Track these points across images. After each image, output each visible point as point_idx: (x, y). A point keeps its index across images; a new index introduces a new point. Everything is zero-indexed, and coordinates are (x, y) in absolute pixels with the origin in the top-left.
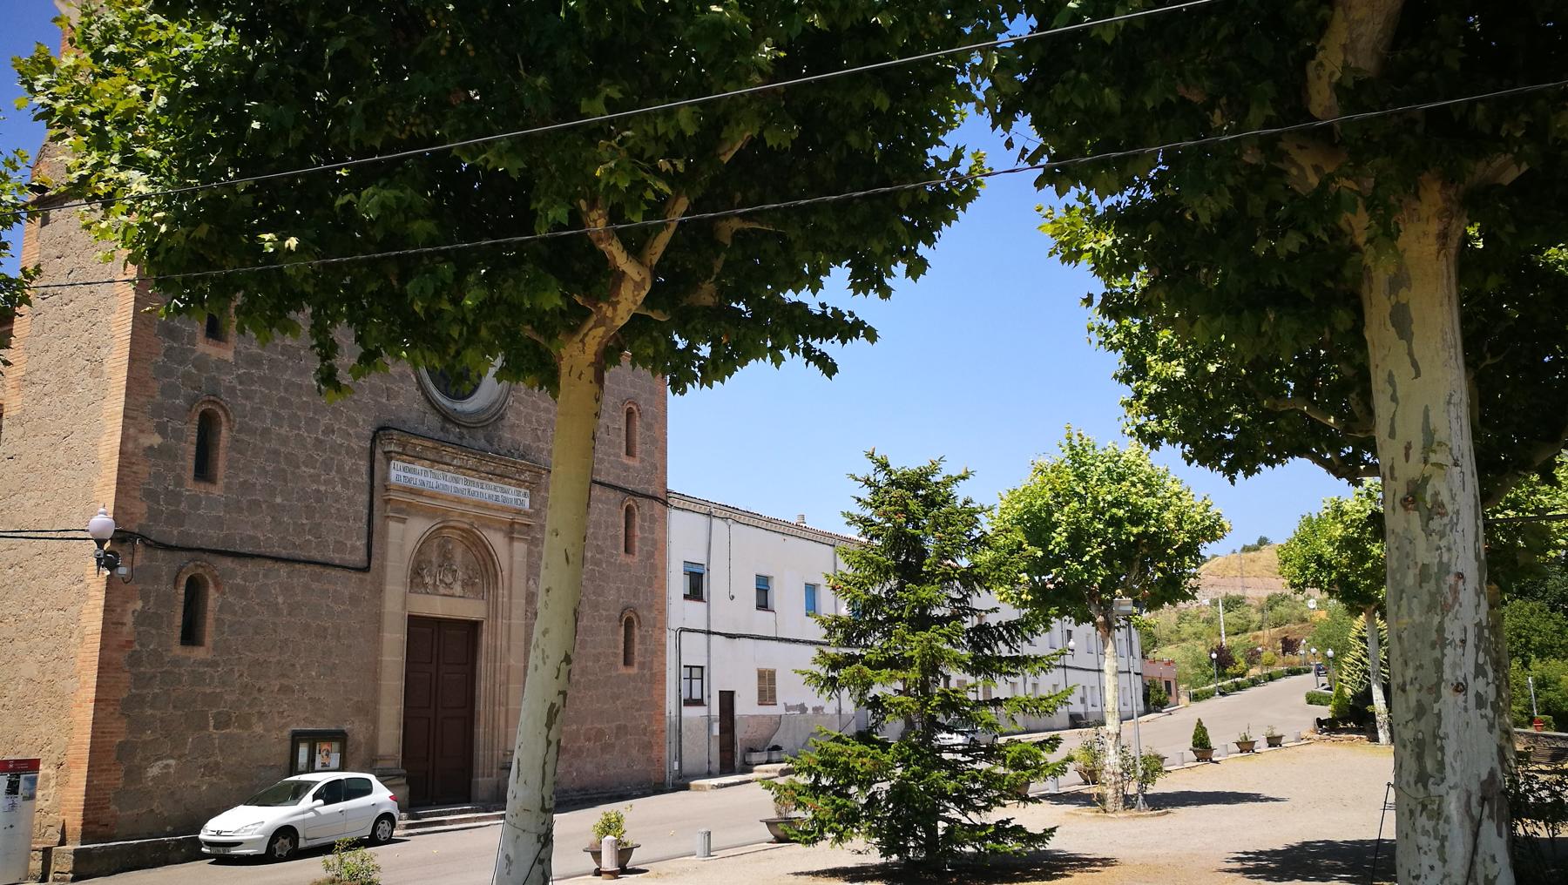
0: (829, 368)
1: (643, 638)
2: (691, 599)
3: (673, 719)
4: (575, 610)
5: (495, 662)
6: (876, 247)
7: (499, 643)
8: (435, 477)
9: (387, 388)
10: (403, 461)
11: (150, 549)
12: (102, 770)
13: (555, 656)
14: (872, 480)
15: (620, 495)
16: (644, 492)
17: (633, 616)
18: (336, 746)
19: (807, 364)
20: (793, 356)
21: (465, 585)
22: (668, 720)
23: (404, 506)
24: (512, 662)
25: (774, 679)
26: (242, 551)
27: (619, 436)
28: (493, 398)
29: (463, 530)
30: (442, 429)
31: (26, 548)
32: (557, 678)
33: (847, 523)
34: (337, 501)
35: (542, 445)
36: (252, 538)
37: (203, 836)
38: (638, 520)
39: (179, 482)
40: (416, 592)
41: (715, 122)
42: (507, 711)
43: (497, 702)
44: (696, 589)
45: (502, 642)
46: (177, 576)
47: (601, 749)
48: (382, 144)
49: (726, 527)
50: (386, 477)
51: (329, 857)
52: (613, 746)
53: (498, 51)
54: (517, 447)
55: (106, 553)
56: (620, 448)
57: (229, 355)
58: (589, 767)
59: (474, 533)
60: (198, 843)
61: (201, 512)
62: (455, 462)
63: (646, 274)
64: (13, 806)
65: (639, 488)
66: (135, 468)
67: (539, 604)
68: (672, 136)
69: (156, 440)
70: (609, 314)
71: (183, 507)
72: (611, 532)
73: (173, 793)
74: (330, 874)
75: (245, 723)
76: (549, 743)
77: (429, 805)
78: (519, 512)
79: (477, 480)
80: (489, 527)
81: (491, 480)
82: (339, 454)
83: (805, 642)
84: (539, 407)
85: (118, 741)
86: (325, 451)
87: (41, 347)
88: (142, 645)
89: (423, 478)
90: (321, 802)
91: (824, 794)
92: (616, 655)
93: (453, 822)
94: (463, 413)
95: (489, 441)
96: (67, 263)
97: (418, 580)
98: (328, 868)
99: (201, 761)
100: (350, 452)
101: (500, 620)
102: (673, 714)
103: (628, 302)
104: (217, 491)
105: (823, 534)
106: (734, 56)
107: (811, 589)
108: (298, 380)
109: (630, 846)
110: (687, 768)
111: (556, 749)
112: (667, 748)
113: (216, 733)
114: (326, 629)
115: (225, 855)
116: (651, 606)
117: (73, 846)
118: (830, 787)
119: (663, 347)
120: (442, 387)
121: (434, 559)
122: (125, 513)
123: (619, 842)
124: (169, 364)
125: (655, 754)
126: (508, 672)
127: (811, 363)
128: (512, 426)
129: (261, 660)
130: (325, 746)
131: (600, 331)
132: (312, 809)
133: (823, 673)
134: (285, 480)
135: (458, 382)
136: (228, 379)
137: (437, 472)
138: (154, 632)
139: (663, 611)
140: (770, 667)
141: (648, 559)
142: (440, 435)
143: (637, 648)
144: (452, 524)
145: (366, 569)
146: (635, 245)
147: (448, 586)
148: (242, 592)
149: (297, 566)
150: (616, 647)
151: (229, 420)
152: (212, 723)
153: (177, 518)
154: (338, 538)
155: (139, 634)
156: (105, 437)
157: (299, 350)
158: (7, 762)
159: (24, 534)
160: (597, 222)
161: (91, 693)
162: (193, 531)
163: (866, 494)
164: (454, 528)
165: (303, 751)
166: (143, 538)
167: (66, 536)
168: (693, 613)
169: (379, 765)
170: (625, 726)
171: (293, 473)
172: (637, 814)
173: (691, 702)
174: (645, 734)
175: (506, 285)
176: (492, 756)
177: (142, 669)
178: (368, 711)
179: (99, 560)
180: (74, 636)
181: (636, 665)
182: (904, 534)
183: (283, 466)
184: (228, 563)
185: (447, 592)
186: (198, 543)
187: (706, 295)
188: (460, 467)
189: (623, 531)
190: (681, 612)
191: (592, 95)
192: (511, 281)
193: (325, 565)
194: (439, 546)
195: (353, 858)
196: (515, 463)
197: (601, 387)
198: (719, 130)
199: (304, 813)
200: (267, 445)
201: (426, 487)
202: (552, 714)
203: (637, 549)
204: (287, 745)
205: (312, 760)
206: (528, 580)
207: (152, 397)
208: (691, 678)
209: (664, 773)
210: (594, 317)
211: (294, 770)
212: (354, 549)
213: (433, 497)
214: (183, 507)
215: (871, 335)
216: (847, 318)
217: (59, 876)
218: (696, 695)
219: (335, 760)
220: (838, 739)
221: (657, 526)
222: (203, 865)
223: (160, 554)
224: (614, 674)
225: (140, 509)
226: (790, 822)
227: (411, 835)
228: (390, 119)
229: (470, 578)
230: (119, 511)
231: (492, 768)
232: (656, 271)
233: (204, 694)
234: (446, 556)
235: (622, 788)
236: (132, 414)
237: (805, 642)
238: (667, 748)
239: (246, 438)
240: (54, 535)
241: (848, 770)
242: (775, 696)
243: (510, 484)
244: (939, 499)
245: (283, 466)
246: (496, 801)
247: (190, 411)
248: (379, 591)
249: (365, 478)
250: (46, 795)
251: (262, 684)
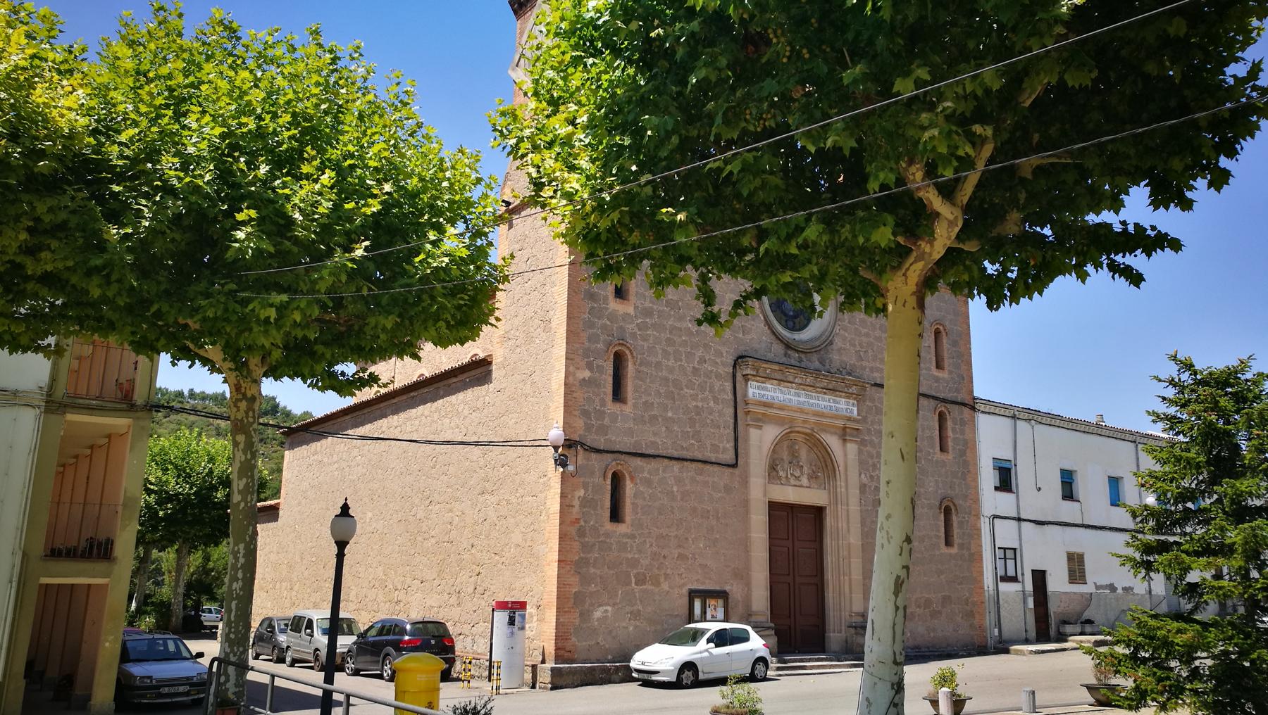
0: (1135, 278)
1: (961, 524)
2: (1001, 491)
3: (991, 592)
4: (912, 499)
5: (838, 540)
6: (1177, 164)
7: (840, 525)
8: (782, 392)
9: (742, 326)
10: (757, 381)
11: (587, 453)
12: (566, 612)
13: (898, 537)
14: (1177, 380)
15: (933, 402)
16: (954, 399)
17: (951, 505)
18: (721, 602)
19: (1113, 277)
20: (1097, 271)
21: (810, 478)
22: (986, 594)
23: (760, 416)
24: (852, 540)
25: (1083, 561)
26: (647, 452)
27: (929, 353)
28: (822, 329)
29: (806, 434)
30: (785, 355)
31: (512, 453)
32: (900, 555)
33: (1153, 421)
34: (710, 414)
35: (865, 364)
36: (653, 443)
37: (633, 664)
38: (949, 424)
39: (603, 403)
40: (773, 483)
41: (1016, 79)
42: (850, 580)
43: (842, 572)
44: (1005, 481)
45: (843, 525)
46: (605, 472)
47: (930, 615)
48: (738, 135)
49: (1030, 427)
50: (745, 395)
51: (724, 688)
52: (940, 612)
53: (828, 50)
54: (844, 366)
55: (560, 455)
56: (930, 362)
57: (631, 310)
58: (921, 629)
59: (815, 436)
60: (629, 669)
61: (618, 425)
62: (796, 380)
63: (958, 213)
64: (512, 633)
65: (949, 396)
66: (575, 395)
67: (882, 495)
68: (980, 92)
69: (587, 374)
70: (927, 249)
71: (607, 421)
72: (927, 433)
73: (611, 632)
74: (725, 701)
75: (657, 583)
76: (897, 608)
77: (793, 653)
78: (849, 419)
79: (814, 394)
80: (825, 431)
81: (825, 393)
82: (710, 378)
83: (1111, 529)
84: (860, 333)
85: (574, 591)
86: (700, 376)
87: (513, 313)
88: (585, 522)
89: (772, 394)
90: (712, 645)
91: (1145, 665)
92: (938, 537)
93: (812, 667)
94: (801, 342)
95: (822, 362)
96: (526, 253)
97: (774, 473)
98: (723, 697)
99: (628, 609)
100: (718, 376)
101: (840, 506)
102: (991, 588)
103: (943, 237)
104: (628, 409)
105: (1124, 432)
106: (1035, 15)
107: (1114, 482)
108: (678, 325)
109: (962, 697)
110: (1006, 635)
111: (902, 614)
112: (988, 617)
113: (637, 589)
114: (708, 511)
115: (648, 681)
116: (966, 496)
117: (550, 664)
118: (1149, 659)
119: (976, 273)
120: (783, 322)
121: (785, 457)
122: (570, 427)
123: (953, 694)
124: (592, 319)
125: (976, 622)
126: (849, 548)
127: (1117, 276)
128: (839, 350)
129: (664, 534)
130: (713, 602)
131: (920, 265)
132: (707, 650)
133: (1137, 556)
134: (673, 399)
135: (798, 318)
136: (630, 327)
137: (783, 389)
138: (592, 512)
139: (977, 500)
140: (1078, 550)
141: (961, 456)
142: (784, 360)
143: (956, 531)
144: (797, 429)
145: (735, 466)
146: (947, 191)
147: (797, 478)
148: (648, 482)
149: (685, 463)
150: (938, 531)
151: (633, 357)
152: (633, 580)
153: (603, 430)
154: (714, 442)
155: (583, 513)
156: (555, 374)
157: (677, 302)
158: (507, 602)
159: (509, 444)
160: (916, 174)
161: (555, 556)
162: (614, 438)
163: (1171, 392)
164: (798, 432)
165: (697, 605)
166: (582, 444)
167: (535, 444)
168: (1003, 504)
169: (753, 619)
170: (949, 597)
171: (678, 394)
172: (968, 669)
173: (1006, 579)
174: (967, 604)
175: (844, 230)
176: (840, 615)
177: (587, 539)
178: (743, 576)
179: (556, 460)
180: (543, 515)
181: (956, 546)
182: (1215, 429)
183: (672, 389)
184: (638, 462)
185: (797, 483)
186: (617, 448)
187: (1012, 225)
188: (801, 384)
189: (937, 432)
190: (992, 501)
191: (907, 74)
192: (848, 226)
193: (705, 462)
194: (788, 447)
195: (743, 690)
196: (844, 379)
197: (923, 312)
198: (1021, 81)
199: (701, 652)
200: (660, 374)
201: (776, 401)
202: (898, 585)
203: (950, 449)
204: (686, 600)
205: (704, 612)
206: (860, 475)
207: (583, 344)
208: (1005, 558)
209: (986, 637)
210: (914, 254)
211: (691, 619)
212: (725, 450)
213: (781, 408)
214: (607, 421)
215: (1176, 245)
216: (1149, 232)
217: (542, 685)
218: (1011, 573)
219: (720, 613)
220: (1155, 617)
221: (967, 429)
222: (633, 686)
223: (594, 456)
224: (937, 553)
225: (579, 423)
226: (1112, 688)
227: (780, 675)
228: (748, 117)
229: (814, 472)
230: (567, 426)
231: (841, 626)
232: (967, 209)
233: (627, 559)
234: (794, 455)
235: (949, 648)
236: (572, 356)
237: (1111, 529)
238: (988, 617)
239: (646, 370)
240: (527, 443)
241: (1167, 644)
242: (1084, 576)
243: (840, 397)
244: (1250, 395)
245: (672, 389)
246: (852, 653)
247: (607, 352)
248: (745, 482)
249: (731, 396)
250: (532, 627)
251: (665, 552)
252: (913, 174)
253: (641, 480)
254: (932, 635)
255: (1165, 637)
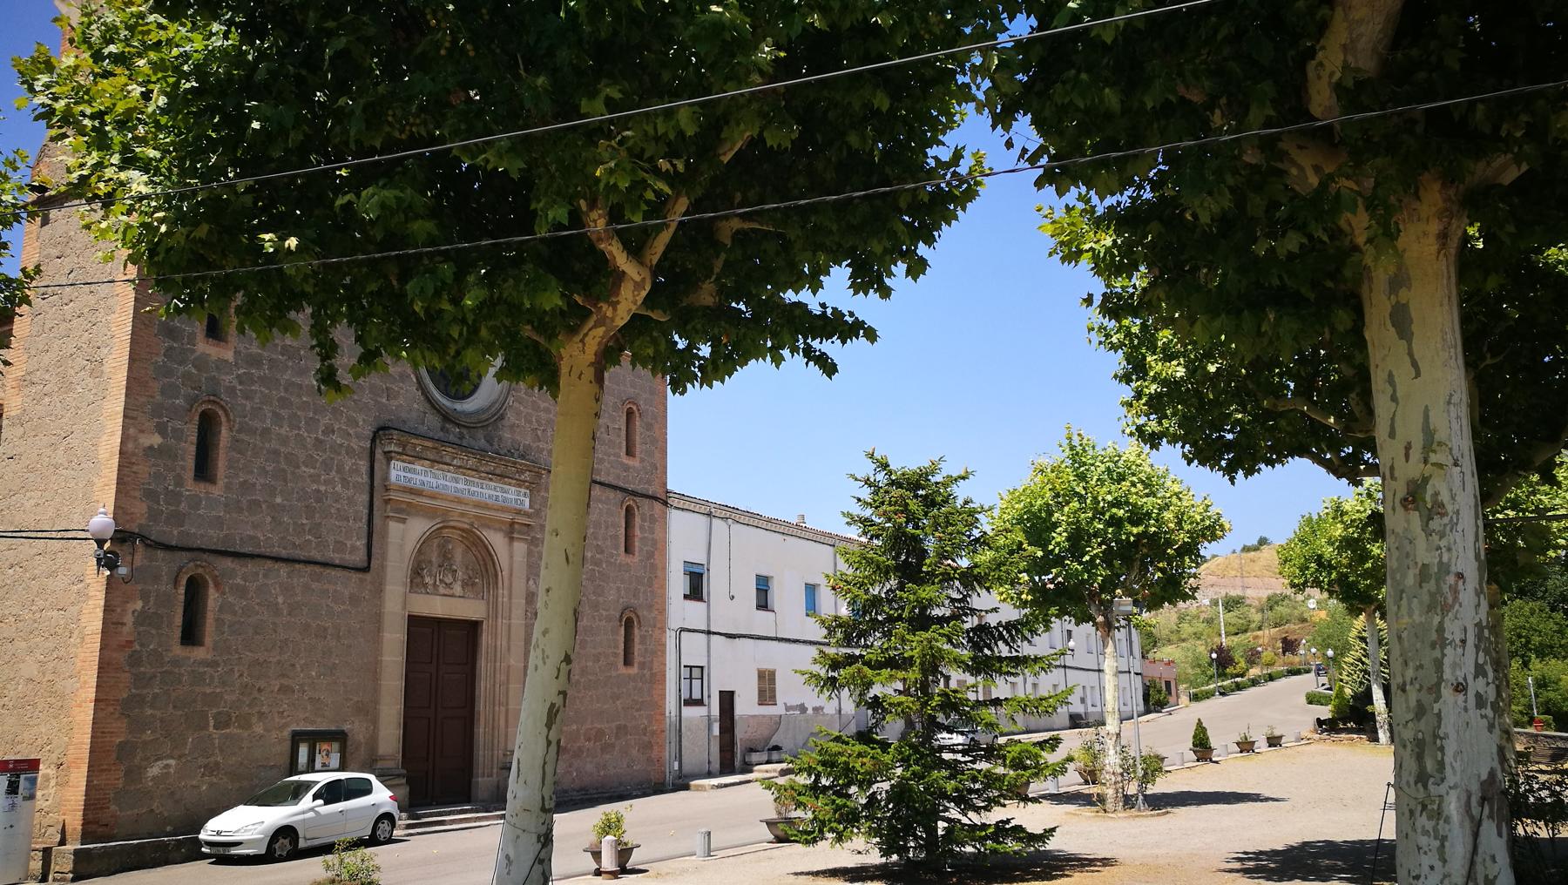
0: (829, 368)
1: (643, 638)
2: (691, 599)
3: (673, 719)
4: (575, 610)
5: (495, 662)
6: (876, 247)
7: (499, 643)
8: (435, 477)
9: (387, 388)
10: (403, 461)
11: (150, 549)
12: (102, 770)
13: (555, 656)
14: (872, 480)
15: (620, 495)
16: (644, 492)
17: (633, 616)
18: (336, 746)
19: (807, 364)
20: (793, 356)
21: (465, 585)
22: (668, 720)
23: (404, 506)
24: (512, 662)
25: (774, 679)
26: (242, 551)
27: (619, 436)
28: (493, 398)
29: (463, 530)
30: (442, 429)
31: (26, 548)
32: (557, 678)
33: (847, 523)
34: (337, 501)
35: (542, 445)
36: (252, 538)
38: (638, 520)
39: (179, 482)
40: (416, 592)
42: (507, 711)
43: (497, 702)
44: (696, 589)
45: (502, 642)
46: (177, 576)
47: (601, 749)
48: (382, 144)
49: (726, 527)
50: (386, 477)
51: (329, 857)
52: (613, 746)
53: (498, 51)
54: (517, 447)
55: (106, 553)
56: (620, 448)
57: (229, 355)
58: (589, 767)
59: (474, 533)
60: (198, 843)
61: (201, 512)
62: (455, 462)
63: (646, 274)
64: (13, 806)
65: (639, 488)
66: (135, 468)
68: (672, 136)
69: (156, 440)
70: (609, 314)
71: (183, 507)
72: (611, 532)
73: (173, 793)
74: (330, 874)
75: (245, 723)
76: (549, 743)
77: (429, 805)
78: (519, 512)
79: (477, 480)
81: (491, 480)
82: (339, 454)
83: (805, 642)
84: (539, 407)
85: (118, 741)
86: (325, 451)
87: (41, 347)
88: (142, 645)
89: (423, 478)
90: (321, 802)
91: (824, 794)
92: (616, 655)
93: (453, 822)
94: (463, 413)
95: (489, 441)
97: (418, 580)
98: (328, 868)
99: (201, 761)
100: (350, 452)
101: (500, 620)
102: (673, 714)
103: (628, 302)
104: (217, 491)
105: (823, 534)
106: (734, 56)
107: (811, 589)
108: (298, 380)
109: (630, 846)
110: (687, 768)
111: (556, 749)
112: (667, 748)
113: (216, 733)
114: (326, 629)
115: (225, 855)
116: (651, 606)
117: (73, 846)
118: (830, 787)
119: (663, 347)
120: (442, 387)
121: (434, 559)
122: (125, 513)
123: (619, 842)
124: (169, 364)
126: (508, 672)
127: (811, 363)
128: (512, 426)
129: (261, 660)
130: (325, 746)
131: (600, 331)
132: (312, 809)
133: (823, 673)
134: (285, 480)
135: (458, 382)
136: (228, 379)
137: (437, 472)
138: (154, 632)
139: (663, 611)
140: (770, 667)
141: (648, 559)
142: (440, 435)
143: (637, 648)
144: (452, 524)
145: (366, 569)
146: (635, 245)
147: (448, 586)
148: (242, 592)
149: (297, 566)
150: (616, 647)
151: (229, 420)
152: (212, 723)
153: (177, 518)
154: (338, 538)
155: (139, 634)
156: (105, 437)
157: (299, 350)
158: (7, 762)
159: (24, 534)
160: (597, 222)
161: (91, 693)
162: (193, 531)
163: (866, 494)
164: (454, 528)
165: (303, 751)
166: (143, 538)
167: (66, 536)
168: (693, 613)
169: (379, 765)
171: (293, 473)
172: (637, 814)
173: (691, 702)
174: (645, 734)
176: (492, 756)
177: (142, 669)
178: (368, 711)
179: (99, 560)
180: (74, 636)
181: (636, 665)
182: (904, 534)
183: (283, 466)
184: (228, 563)
185: (447, 592)
186: (198, 543)
187: (706, 295)
188: (460, 467)
189: (623, 531)
190: (681, 612)
193: (325, 565)
194: (439, 546)
195: (353, 858)
196: (515, 463)
197: (601, 387)
199: (304, 813)
200: (267, 445)
201: (426, 487)
202: (552, 714)
203: (637, 549)
204: (287, 745)
205: (312, 760)
206: (528, 580)
207: (152, 397)
208: (691, 678)
209: (664, 773)
210: (594, 317)
211: (294, 770)
212: (354, 549)
213: (433, 497)
214: (183, 507)
215: (871, 335)
216: (847, 318)
217: (59, 876)
218: (696, 695)
219: (335, 760)
220: (838, 739)
221: (657, 526)
222: (203, 865)
223: (160, 554)
224: (614, 674)
225: (140, 509)
226: (790, 822)
227: (411, 835)
228: (390, 119)
229: (470, 578)
230: (119, 511)
231: (492, 768)
232: (656, 271)
233: (204, 694)
234: (446, 556)
235: (622, 788)
236: (132, 414)
237: (805, 642)
238: (667, 748)
239: (246, 438)
240: (54, 535)
241: (848, 770)
242: (775, 696)
243: (510, 484)
244: (939, 499)
245: (283, 466)
246: (496, 801)
247: (190, 411)
248: (379, 591)
249: (365, 478)
250: (46, 795)
251: (262, 684)
252: (595, 221)
253: (231, 588)
254: (602, 773)
255: (847, 763)
